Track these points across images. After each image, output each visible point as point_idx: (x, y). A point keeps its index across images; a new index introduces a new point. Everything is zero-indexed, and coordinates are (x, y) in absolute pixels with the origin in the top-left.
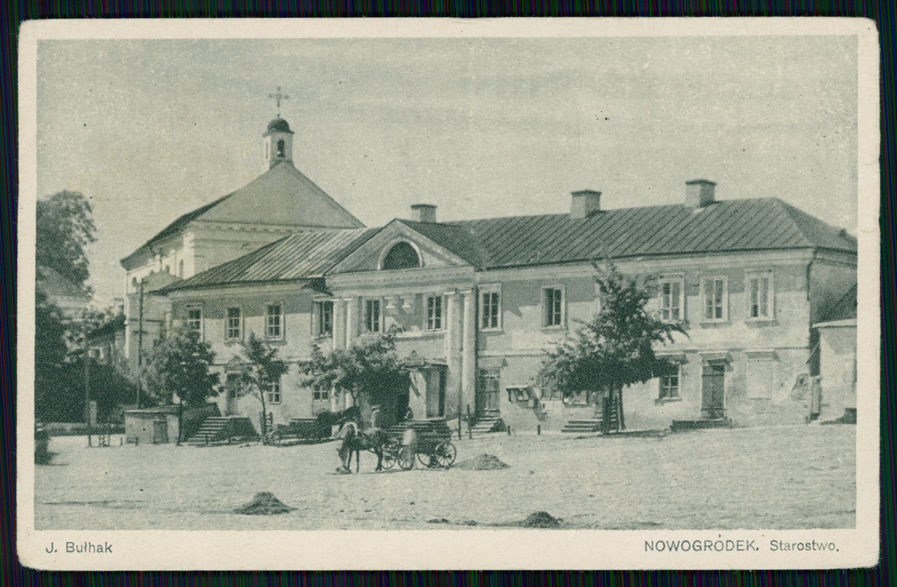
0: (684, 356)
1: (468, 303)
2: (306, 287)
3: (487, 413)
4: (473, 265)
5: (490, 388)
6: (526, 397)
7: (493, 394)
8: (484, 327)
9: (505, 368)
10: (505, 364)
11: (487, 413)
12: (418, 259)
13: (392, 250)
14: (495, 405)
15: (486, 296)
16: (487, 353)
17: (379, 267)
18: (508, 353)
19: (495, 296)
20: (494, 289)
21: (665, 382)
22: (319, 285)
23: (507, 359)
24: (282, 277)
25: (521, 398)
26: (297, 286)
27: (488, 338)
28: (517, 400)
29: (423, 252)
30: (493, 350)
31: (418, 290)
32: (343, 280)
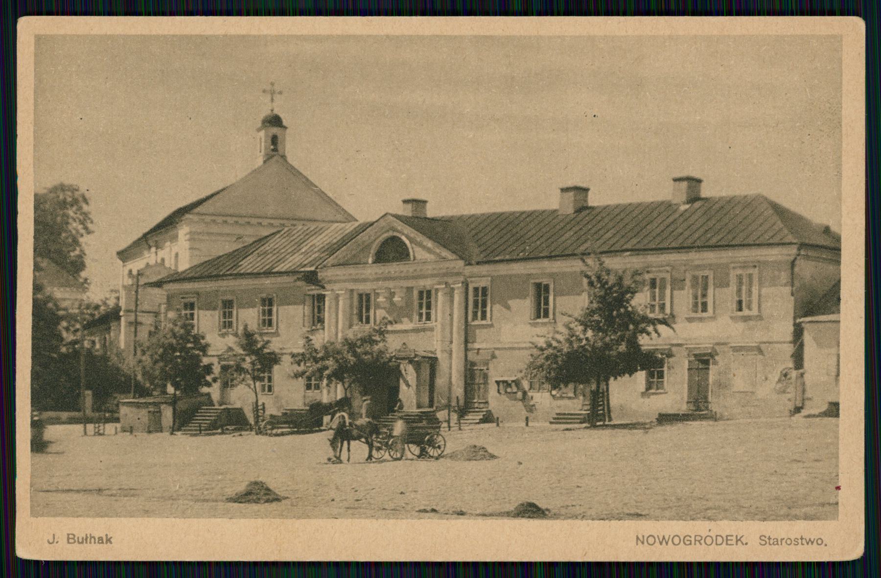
2: (298, 279)
3: (476, 405)
7: (482, 386)
8: (473, 320)
17: (370, 260)
23: (497, 353)
25: (509, 390)
27: (477, 331)
28: (506, 392)
29: (414, 246)
30: (483, 342)
31: (410, 283)
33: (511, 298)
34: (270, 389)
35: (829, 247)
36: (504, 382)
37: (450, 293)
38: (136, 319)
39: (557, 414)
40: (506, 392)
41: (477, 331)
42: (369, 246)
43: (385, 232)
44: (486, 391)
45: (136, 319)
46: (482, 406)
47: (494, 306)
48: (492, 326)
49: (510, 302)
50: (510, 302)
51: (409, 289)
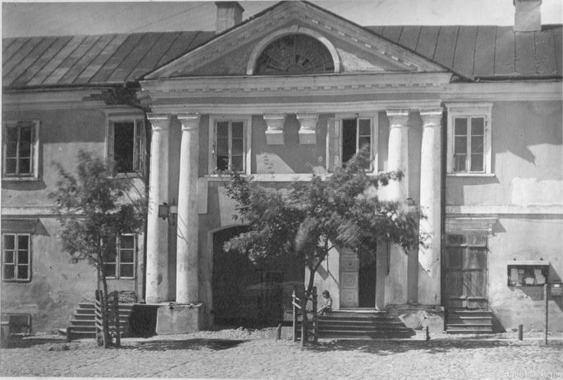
0: (497, 220)
1: (430, 135)
2: (93, 97)
3: (465, 304)
4: (449, 71)
5: (470, 264)
6: (541, 279)
7: (474, 274)
8: (455, 170)
9: (499, 235)
10: (498, 228)
11: (465, 304)
12: (331, 60)
13: (270, 46)
14: (479, 292)
15: (460, 123)
16: (464, 210)
17: (250, 72)
18: (505, 211)
19: (479, 124)
20: (471, 113)
21: (406, 245)
22: (125, 94)
23: (503, 221)
24: (35, 82)
25: (529, 281)
26: (76, 96)
27: (466, 188)
28: (524, 284)
29: (343, 53)
30: (478, 203)
31: (326, 108)
32: (181, 87)
33: (529, 144)
34: (23, 272)
35: (401, 292)
36: (519, 267)
37: (415, 123)
38: (428, 338)
39: (82, 306)
40: (524, 284)
41: (466, 188)
42: (247, 48)
43: (283, 27)
44: (483, 280)
45: (428, 338)
46: (475, 305)
47: (499, 156)
48: (493, 179)
49: (532, 148)
50: (532, 148)
51: (323, 119)
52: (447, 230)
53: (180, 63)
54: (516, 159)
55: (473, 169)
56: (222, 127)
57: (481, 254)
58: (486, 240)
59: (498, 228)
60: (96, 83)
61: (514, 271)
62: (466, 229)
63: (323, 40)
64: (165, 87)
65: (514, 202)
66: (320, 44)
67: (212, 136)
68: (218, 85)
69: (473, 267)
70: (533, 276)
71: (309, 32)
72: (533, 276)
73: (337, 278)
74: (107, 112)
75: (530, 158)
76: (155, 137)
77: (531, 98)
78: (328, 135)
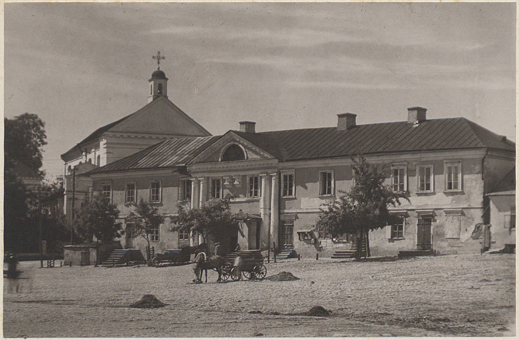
0: (296, 215)
2: (175, 171)
5: (287, 232)
7: (289, 236)
8: (284, 196)
9: (297, 220)
10: (297, 218)
11: (286, 247)
15: (285, 177)
16: (286, 211)
17: (220, 160)
19: (291, 176)
20: (289, 173)
25: (306, 238)
26: (169, 171)
27: (286, 202)
28: (304, 239)
41: (286, 202)
48: (295, 198)
49: (307, 184)
50: (307, 184)
52: (281, 219)
53: (198, 158)
54: (302, 189)
55: (427, 190)
56: (213, 181)
57: (291, 228)
58: (293, 222)
59: (297, 218)
60: (480, 146)
61: (301, 235)
62: (287, 219)
63: (240, 146)
64: (194, 167)
65: (301, 207)
66: (240, 147)
67: (211, 185)
68: (209, 166)
69: (289, 233)
70: (307, 236)
71: (237, 143)
72: (307, 236)
73: (247, 237)
74: (180, 176)
75: (306, 188)
76: (263, 182)
77: (475, 157)
78: (453, 175)
